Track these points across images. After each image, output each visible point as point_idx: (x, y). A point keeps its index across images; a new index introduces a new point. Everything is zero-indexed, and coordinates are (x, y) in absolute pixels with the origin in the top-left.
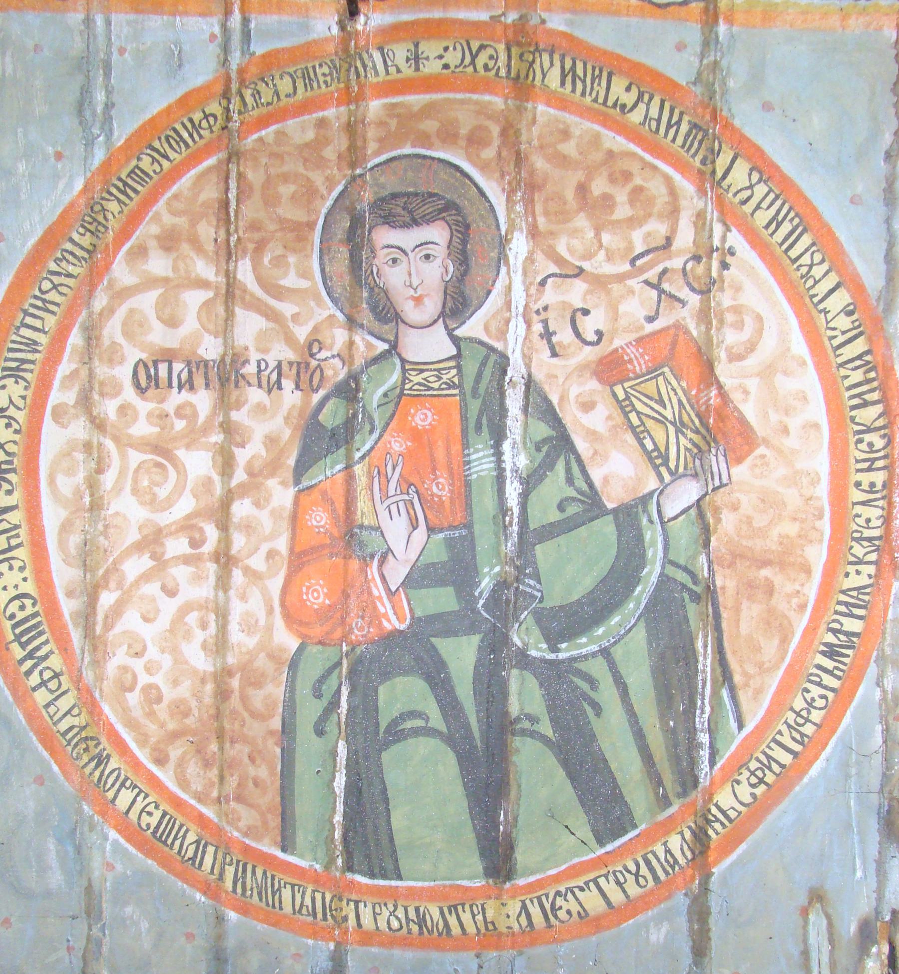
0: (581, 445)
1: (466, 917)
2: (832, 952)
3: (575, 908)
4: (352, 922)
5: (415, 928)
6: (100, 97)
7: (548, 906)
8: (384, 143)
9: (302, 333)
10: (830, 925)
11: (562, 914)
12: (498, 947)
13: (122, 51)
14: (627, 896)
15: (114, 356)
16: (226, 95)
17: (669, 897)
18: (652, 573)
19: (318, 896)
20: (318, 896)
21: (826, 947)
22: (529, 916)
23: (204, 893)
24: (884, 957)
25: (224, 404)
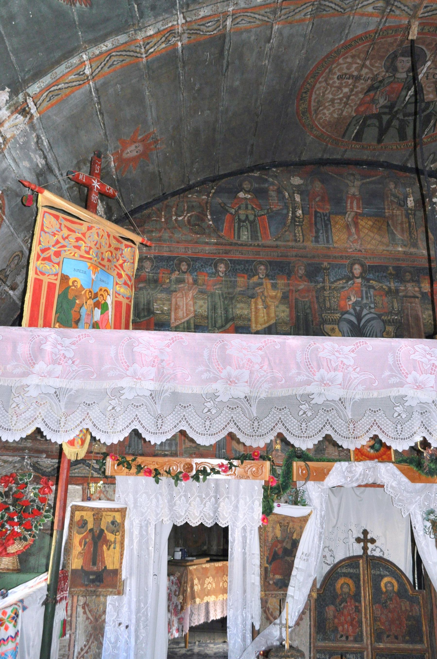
0: (425, 92)
6: (347, 31)
8: (415, 245)
9: (376, 73)
13: (355, 23)
15: (335, 73)
16: (376, 33)
18: (428, 111)
25: (355, 82)
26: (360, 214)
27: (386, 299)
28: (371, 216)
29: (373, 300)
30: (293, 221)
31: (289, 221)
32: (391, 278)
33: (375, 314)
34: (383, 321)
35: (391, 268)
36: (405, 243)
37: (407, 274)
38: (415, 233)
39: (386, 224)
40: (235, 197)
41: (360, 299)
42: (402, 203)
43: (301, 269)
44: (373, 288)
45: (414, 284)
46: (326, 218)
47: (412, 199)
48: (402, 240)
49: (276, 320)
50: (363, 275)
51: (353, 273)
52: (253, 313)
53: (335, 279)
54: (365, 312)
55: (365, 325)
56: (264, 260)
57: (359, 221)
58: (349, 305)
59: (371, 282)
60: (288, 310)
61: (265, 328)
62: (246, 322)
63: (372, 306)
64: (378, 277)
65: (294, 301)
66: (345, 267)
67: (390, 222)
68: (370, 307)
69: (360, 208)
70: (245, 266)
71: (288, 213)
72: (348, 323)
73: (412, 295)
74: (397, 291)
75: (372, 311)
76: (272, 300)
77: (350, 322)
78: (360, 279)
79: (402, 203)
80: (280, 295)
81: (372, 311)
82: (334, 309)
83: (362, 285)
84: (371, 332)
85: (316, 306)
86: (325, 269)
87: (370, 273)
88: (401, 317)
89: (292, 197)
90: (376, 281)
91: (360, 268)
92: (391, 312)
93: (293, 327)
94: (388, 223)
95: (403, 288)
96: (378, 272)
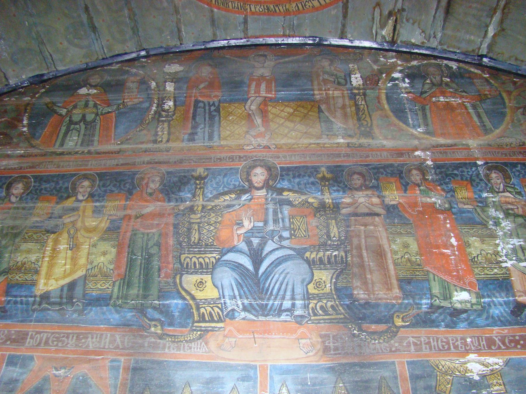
1: (281, 8)
2: (380, 19)
3: (311, 5)
4: (249, 10)
5: (266, 11)
7: (303, 5)
10: (381, 11)
11: (307, 7)
12: (290, 15)
14: (320, 4)
17: (337, 3)
19: (239, 4)
20: (239, 4)
21: (379, 17)
22: (298, 7)
23: (207, 5)
24: (394, 20)
26: (271, 99)
27: (314, 222)
28: (290, 101)
29: (287, 224)
30: (157, 116)
31: (150, 117)
32: (324, 186)
33: (291, 249)
34: (307, 261)
35: (323, 169)
36: (350, 133)
37: (356, 176)
38: (368, 119)
39: (316, 110)
40: (73, 95)
41: (261, 224)
42: (343, 81)
43: (153, 181)
44: (289, 203)
45: (369, 192)
46: (213, 108)
47: (358, 75)
48: (345, 129)
49: (87, 270)
50: (271, 183)
51: (250, 181)
52: (47, 259)
53: (215, 193)
54: (270, 246)
55: (268, 273)
56: (91, 172)
57: (270, 108)
58: (239, 236)
59: (285, 193)
60: (114, 251)
61: (63, 287)
62: (28, 277)
63: (286, 234)
64: (299, 184)
65: (129, 234)
66: (237, 173)
67: (323, 107)
68: (281, 237)
69: (271, 91)
70: (57, 183)
71: (151, 105)
72: (234, 270)
73: (366, 211)
74: (336, 207)
75: (285, 243)
76: (86, 235)
77: (237, 267)
78: (264, 190)
79: (343, 81)
80: (104, 225)
81: (285, 243)
82: (207, 245)
83: (266, 199)
84: (281, 284)
85: (171, 241)
86: (200, 178)
87: (283, 179)
88: (346, 252)
89: (161, 87)
90: (295, 192)
91: (266, 173)
92: (325, 244)
93: (117, 283)
94: (319, 107)
95: (348, 200)
96: (299, 176)
